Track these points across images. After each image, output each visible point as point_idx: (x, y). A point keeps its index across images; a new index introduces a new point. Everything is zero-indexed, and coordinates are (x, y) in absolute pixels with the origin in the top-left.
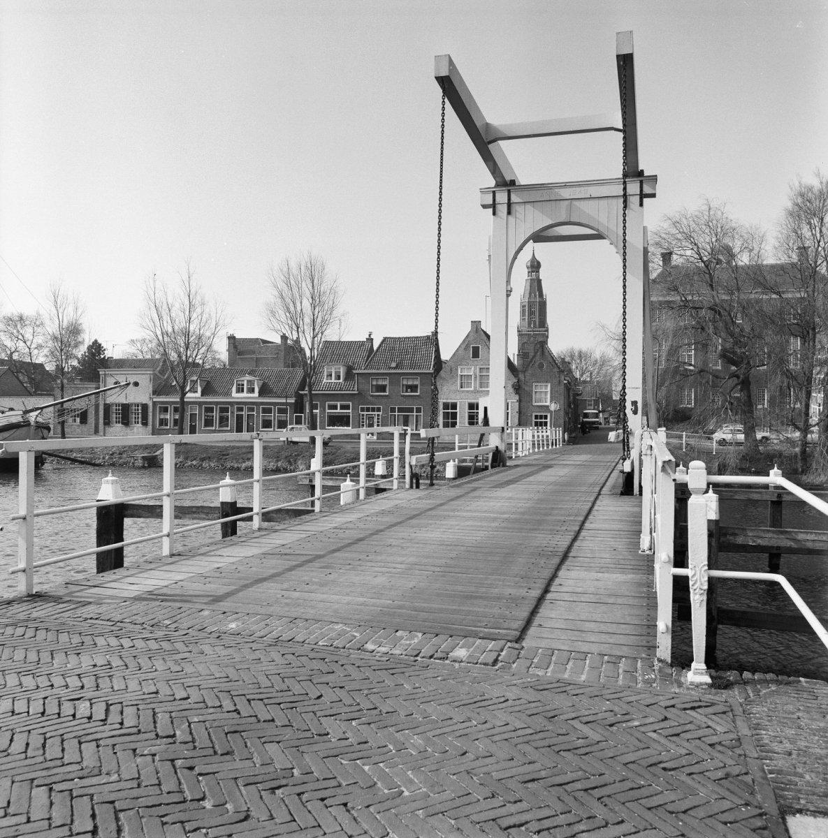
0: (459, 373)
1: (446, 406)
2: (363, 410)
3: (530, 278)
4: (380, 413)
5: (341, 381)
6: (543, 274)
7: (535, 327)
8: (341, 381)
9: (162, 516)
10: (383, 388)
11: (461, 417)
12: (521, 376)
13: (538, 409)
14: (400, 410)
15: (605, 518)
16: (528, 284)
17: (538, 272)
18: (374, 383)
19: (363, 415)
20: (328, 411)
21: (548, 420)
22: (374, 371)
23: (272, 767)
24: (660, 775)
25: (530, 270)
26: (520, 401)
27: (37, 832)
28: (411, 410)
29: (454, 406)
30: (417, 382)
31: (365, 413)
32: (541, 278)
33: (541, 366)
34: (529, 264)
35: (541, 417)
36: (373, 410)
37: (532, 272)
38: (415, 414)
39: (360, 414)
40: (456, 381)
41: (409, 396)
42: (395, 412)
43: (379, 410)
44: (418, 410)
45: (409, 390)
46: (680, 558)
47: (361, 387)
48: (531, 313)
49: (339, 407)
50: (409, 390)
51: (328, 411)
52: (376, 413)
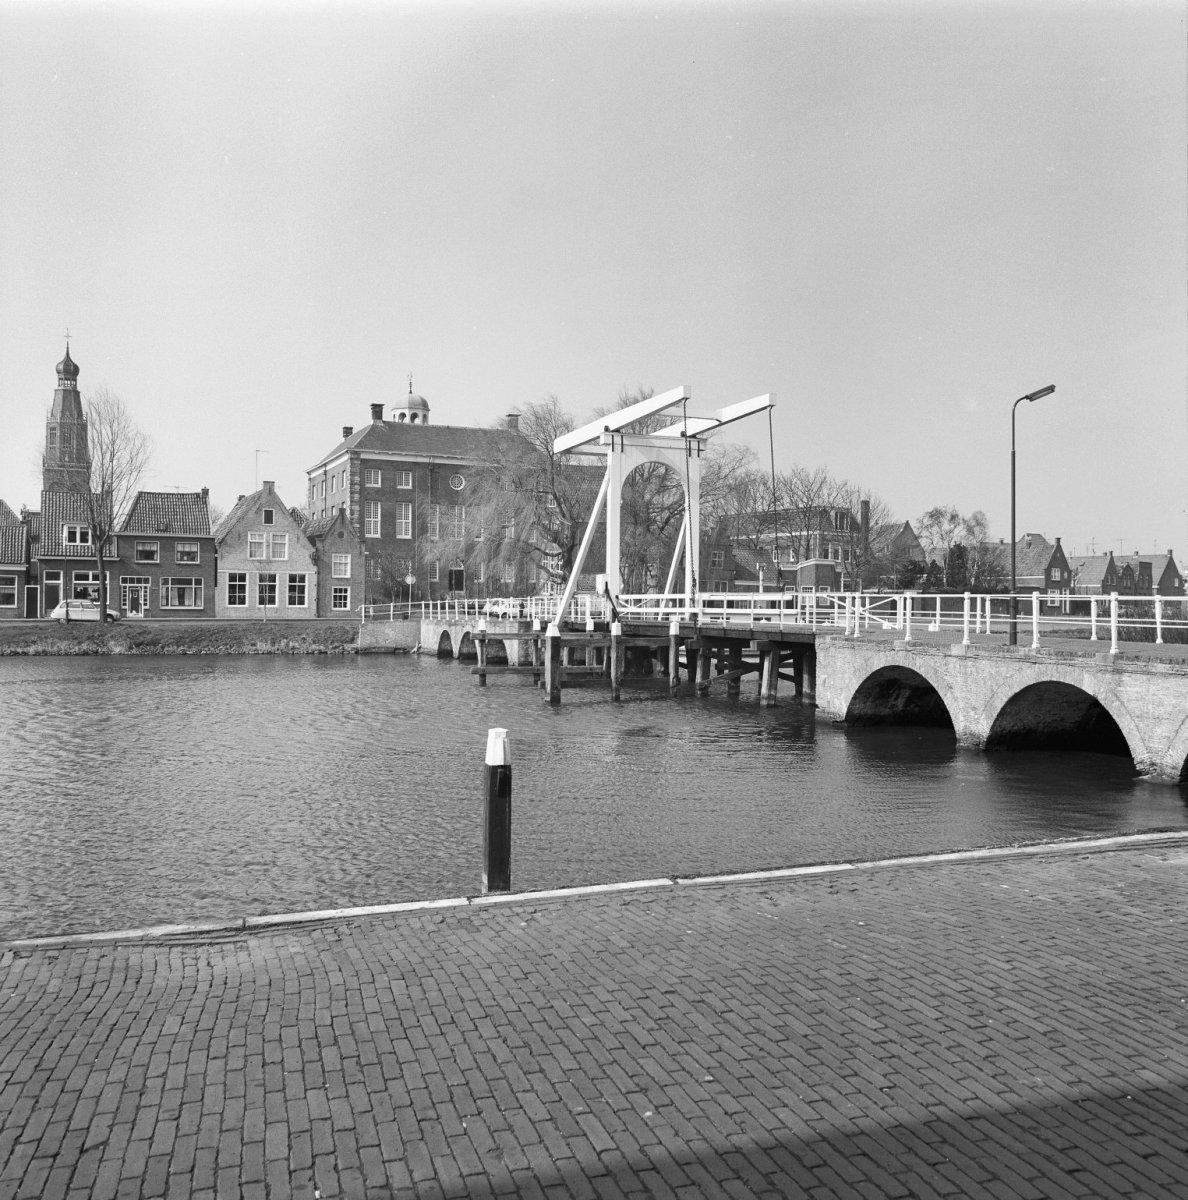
0: (249, 539)
1: (232, 577)
2: (125, 581)
3: (62, 388)
4: (149, 585)
5: (90, 543)
6: (82, 383)
7: (71, 460)
8: (90, 543)
9: (680, 627)
10: (149, 555)
11: (281, 593)
12: (319, 545)
13: (336, 582)
14: (174, 582)
15: (64, 773)
16: (61, 397)
17: (75, 380)
18: (140, 548)
19: (125, 588)
20: (45, 582)
21: (349, 594)
22: (137, 534)
23: (271, 1026)
24: (319, 1185)
25: (62, 376)
26: (319, 573)
27: (45, 1184)
28: (189, 582)
29: (242, 578)
30: (194, 549)
31: (128, 585)
32: (79, 389)
33: (341, 535)
34: (61, 367)
35: (341, 591)
36: (139, 581)
37: (66, 379)
38: (193, 586)
39: (120, 587)
40: (246, 548)
41: (186, 565)
42: (191, 584)
43: (146, 581)
44: (198, 582)
45: (185, 558)
46: (905, 609)
47: (122, 552)
48: (65, 440)
49: (91, 577)
50: (185, 558)
51: (45, 582)
52: (143, 585)
